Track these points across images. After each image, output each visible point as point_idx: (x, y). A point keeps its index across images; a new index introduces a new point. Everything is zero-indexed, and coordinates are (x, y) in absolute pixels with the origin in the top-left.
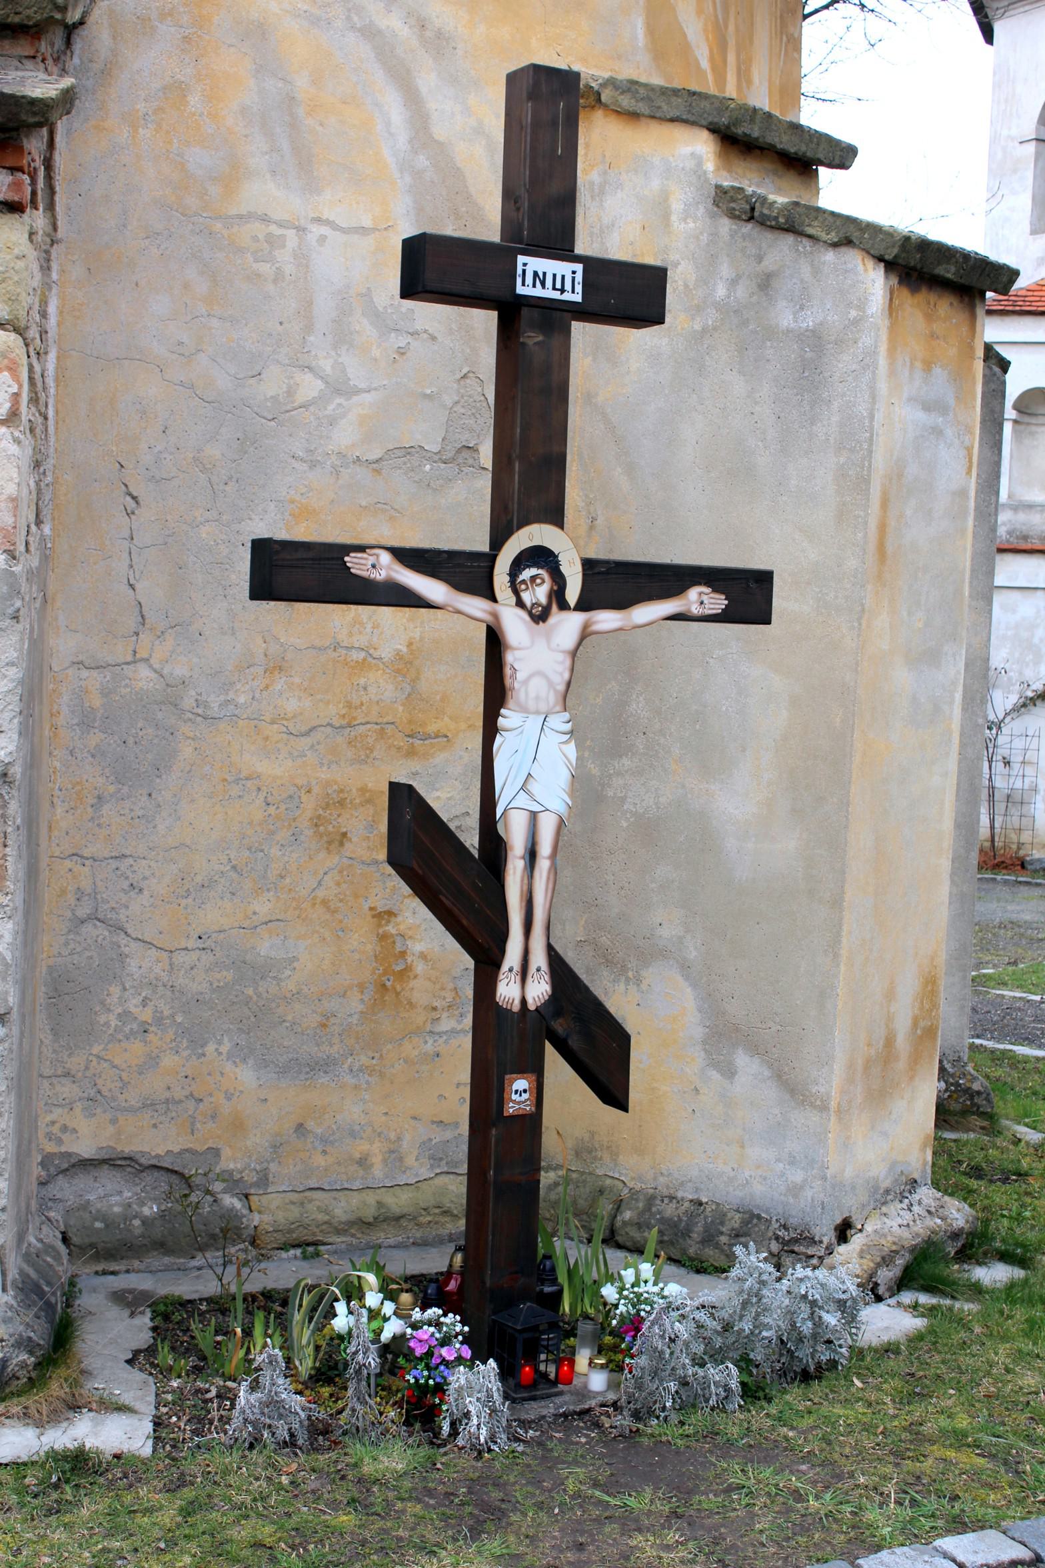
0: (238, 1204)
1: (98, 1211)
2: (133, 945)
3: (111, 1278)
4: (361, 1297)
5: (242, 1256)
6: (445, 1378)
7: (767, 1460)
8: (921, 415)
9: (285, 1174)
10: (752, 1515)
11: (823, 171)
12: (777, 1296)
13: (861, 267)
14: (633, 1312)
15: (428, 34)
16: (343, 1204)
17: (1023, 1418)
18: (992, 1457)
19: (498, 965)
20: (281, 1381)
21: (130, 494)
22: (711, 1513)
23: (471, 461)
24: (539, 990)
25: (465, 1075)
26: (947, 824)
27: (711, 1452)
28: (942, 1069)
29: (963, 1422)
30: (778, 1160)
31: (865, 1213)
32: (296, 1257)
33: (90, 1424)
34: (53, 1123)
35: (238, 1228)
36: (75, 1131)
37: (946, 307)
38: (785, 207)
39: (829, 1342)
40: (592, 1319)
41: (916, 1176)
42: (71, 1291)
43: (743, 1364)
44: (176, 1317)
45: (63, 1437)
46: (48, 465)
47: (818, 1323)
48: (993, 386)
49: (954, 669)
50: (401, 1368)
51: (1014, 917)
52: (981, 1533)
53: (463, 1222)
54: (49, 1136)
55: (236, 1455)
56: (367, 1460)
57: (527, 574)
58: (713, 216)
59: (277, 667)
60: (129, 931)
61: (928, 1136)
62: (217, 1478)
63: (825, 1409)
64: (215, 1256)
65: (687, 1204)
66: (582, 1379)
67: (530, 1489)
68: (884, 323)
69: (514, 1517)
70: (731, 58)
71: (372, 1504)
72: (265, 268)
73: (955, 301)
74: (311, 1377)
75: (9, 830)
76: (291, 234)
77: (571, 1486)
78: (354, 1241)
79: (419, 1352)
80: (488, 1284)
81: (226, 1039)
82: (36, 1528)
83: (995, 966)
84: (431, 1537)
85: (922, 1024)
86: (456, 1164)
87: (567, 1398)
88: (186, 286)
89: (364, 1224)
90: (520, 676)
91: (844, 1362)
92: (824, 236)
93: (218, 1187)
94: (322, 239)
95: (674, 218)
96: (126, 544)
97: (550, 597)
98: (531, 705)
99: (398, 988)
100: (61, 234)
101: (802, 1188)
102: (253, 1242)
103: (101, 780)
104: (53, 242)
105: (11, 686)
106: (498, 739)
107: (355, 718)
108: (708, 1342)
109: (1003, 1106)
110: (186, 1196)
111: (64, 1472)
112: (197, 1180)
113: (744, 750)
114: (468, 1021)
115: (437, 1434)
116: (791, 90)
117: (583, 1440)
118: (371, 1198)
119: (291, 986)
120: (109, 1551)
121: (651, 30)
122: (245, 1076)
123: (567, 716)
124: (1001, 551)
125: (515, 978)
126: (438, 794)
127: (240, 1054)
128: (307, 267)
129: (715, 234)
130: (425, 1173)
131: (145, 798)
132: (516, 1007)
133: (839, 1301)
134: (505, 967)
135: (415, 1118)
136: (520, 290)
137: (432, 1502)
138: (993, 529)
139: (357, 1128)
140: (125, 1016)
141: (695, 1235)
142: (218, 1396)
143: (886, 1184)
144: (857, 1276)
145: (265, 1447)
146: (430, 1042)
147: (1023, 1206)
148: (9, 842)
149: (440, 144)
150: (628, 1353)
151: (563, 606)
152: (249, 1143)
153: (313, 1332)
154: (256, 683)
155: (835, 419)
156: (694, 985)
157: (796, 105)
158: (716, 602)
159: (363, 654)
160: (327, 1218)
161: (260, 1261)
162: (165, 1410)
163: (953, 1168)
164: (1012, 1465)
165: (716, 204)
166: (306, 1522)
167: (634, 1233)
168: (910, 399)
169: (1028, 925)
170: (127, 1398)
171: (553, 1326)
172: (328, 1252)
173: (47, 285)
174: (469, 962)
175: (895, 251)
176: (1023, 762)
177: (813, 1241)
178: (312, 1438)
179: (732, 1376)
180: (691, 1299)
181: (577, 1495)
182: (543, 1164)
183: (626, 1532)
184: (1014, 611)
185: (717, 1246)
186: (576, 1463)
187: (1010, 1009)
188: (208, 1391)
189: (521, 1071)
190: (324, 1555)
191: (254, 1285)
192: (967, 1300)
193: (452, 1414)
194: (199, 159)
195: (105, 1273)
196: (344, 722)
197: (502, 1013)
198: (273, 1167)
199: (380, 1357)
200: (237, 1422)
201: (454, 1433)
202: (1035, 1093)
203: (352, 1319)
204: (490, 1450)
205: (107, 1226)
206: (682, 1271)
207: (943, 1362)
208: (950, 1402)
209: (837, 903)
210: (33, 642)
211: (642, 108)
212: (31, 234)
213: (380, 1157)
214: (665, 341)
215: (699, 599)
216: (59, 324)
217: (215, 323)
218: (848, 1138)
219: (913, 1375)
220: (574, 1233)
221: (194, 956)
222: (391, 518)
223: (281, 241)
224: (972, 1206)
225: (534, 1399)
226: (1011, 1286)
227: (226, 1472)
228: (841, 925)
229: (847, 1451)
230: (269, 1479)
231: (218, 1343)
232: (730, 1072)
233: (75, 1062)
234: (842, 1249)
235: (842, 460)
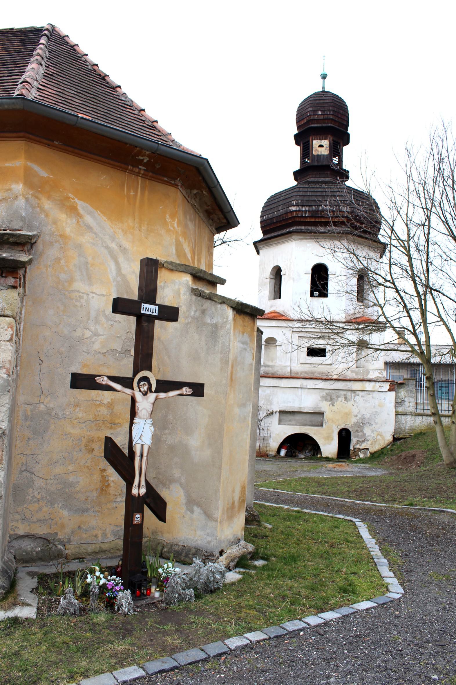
0: (62, 548)
1: (24, 550)
2: (36, 478)
3: (27, 568)
4: (95, 573)
5: (63, 562)
6: (116, 595)
7: (201, 615)
8: (241, 345)
9: (75, 539)
10: (197, 630)
11: (218, 285)
12: (204, 571)
13: (227, 309)
14: (166, 576)
15: (122, 248)
16: (90, 547)
17: (266, 601)
18: (259, 611)
19: (132, 484)
20: (72, 597)
21: (40, 360)
22: (186, 630)
23: (129, 354)
24: (143, 491)
25: (123, 513)
26: (248, 447)
27: (186, 613)
28: (247, 510)
29: (251, 603)
30: (205, 535)
31: (227, 548)
32: (77, 562)
33: (19, 609)
34: (13, 526)
35: (62, 554)
36: (18, 528)
37: (247, 319)
38: (209, 294)
39: (217, 582)
40: (156, 578)
41: (240, 538)
42: (16, 572)
43: (195, 589)
44: (44, 579)
45: (11, 614)
46: (20, 352)
47: (215, 577)
48: (259, 338)
49: (249, 408)
50: (105, 592)
51: (265, 469)
52: (256, 632)
53: (122, 552)
54: (12, 529)
55: (59, 617)
56: (95, 618)
57: (142, 383)
58: (191, 295)
59: (77, 405)
60: (35, 474)
61: (243, 528)
62: (54, 624)
63: (216, 600)
64: (55, 562)
65: (181, 547)
66: (153, 594)
67: (138, 625)
68: (232, 323)
69: (134, 633)
70: (196, 257)
71: (96, 630)
72: (78, 304)
73: (250, 318)
74: (80, 595)
75: (4, 447)
76: (85, 296)
77: (149, 624)
78: (93, 557)
79: (109, 588)
80: (128, 569)
81: (60, 503)
82: (3, 640)
83: (260, 482)
84: (112, 639)
85: (241, 499)
86: (121, 536)
87: (149, 599)
88: (58, 308)
89: (95, 553)
90: (139, 409)
91: (221, 588)
92: (218, 301)
93: (57, 543)
94: (93, 297)
95: (181, 295)
96: (39, 372)
97: (148, 389)
98: (142, 417)
99: (106, 490)
100: (26, 293)
101: (211, 542)
102: (66, 558)
103: (29, 434)
104: (24, 296)
105: (6, 409)
106: (134, 426)
107: (97, 419)
108: (186, 583)
109: (262, 519)
110: (48, 546)
111: (11, 624)
112: (51, 541)
113: (197, 428)
114: (124, 498)
115: (114, 610)
116: (210, 265)
117: (153, 611)
118: (98, 546)
119: (78, 489)
120: (23, 646)
121: (177, 250)
122: (65, 513)
123: (151, 420)
124: (261, 377)
125: (137, 488)
126: (118, 439)
127: (64, 507)
128: (89, 304)
129: (191, 300)
130: (112, 539)
131: (41, 438)
132: (137, 495)
133: (220, 572)
134: (134, 485)
135: (110, 524)
136: (142, 312)
137: (112, 629)
138: (259, 373)
139: (95, 527)
140: (33, 497)
141: (183, 555)
142: (55, 601)
143: (232, 540)
144: (225, 565)
145: (67, 615)
146: (114, 504)
147: (267, 545)
148: (4, 451)
149: (124, 275)
150: (165, 587)
151: (151, 392)
152: (65, 531)
153: (81, 583)
154: (71, 409)
155: (220, 346)
156: (184, 489)
157: (212, 268)
158: (190, 391)
159: (99, 402)
160: (86, 551)
161: (67, 563)
162: (40, 605)
163: (249, 535)
164: (263, 613)
165: (192, 292)
166: (78, 636)
167: (168, 555)
168: (238, 341)
169: (269, 471)
170: (30, 602)
171: (146, 580)
172: (86, 561)
173: (22, 306)
175: (235, 305)
176: (267, 430)
177: (213, 556)
178: (80, 612)
179: (192, 592)
180: (182, 572)
181: (151, 626)
182: (143, 536)
183: (164, 636)
184: (265, 392)
185: (189, 557)
186: (151, 617)
187: (264, 493)
188: (52, 599)
189: (138, 512)
190: (82, 645)
191: (66, 570)
192: (253, 570)
193: (118, 605)
194: (63, 276)
195: (25, 567)
196: (94, 420)
197: (133, 497)
199: (99, 589)
200: (60, 608)
201: (119, 610)
202: (270, 515)
203: (92, 579)
204: (128, 614)
205: (26, 554)
206: (180, 564)
207: (247, 587)
208: (248, 597)
209: (220, 468)
210: (13, 398)
211: (174, 268)
212: (19, 294)
213: (100, 535)
214: (178, 325)
215: (185, 390)
216: (25, 316)
217: (65, 317)
218: (223, 528)
219: (239, 590)
220: (151, 555)
221: (52, 481)
222: (108, 367)
224: (254, 545)
225: (140, 600)
226: (264, 566)
227: (56, 622)
228: (221, 474)
229: (222, 611)
230: (68, 624)
231: (56, 586)
232: (192, 512)
233: (20, 509)
234: (221, 558)
235: (222, 356)
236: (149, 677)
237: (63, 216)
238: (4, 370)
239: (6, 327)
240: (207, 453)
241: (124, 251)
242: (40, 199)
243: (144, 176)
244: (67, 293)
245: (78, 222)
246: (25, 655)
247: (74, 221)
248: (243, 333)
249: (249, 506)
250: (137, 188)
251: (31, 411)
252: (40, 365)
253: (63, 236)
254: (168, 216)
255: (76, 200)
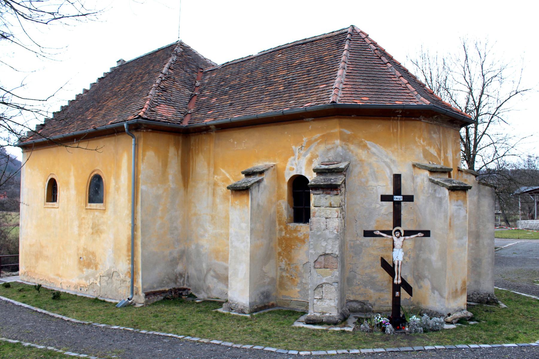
0: (371, 307)
8: (456, 207)
9: (377, 304)
24: (400, 282)
37: (460, 193)
42: (349, 316)
45: (343, 329)
54: (347, 297)
57: (396, 233)
72: (372, 192)
76: (375, 188)
85: (463, 288)
94: (379, 188)
95: (425, 182)
122: (372, 291)
127: (371, 288)
129: (429, 184)
132: (397, 283)
134: (395, 279)
140: (356, 283)
151: (401, 236)
158: (422, 235)
174: (392, 278)
194: (363, 180)
198: (376, 303)
209: (446, 271)
211: (420, 167)
223: (374, 188)
232: (434, 293)
233: (350, 288)
236: (386, 353)
237: (360, 151)
238: (336, 230)
239: (335, 212)
240: (440, 263)
241: (393, 162)
242: (348, 145)
243: (401, 120)
244: (366, 188)
245: (368, 152)
246: (345, 341)
247: (366, 152)
248: (457, 200)
249: (491, 294)
250: (398, 127)
251: (353, 244)
252: (356, 223)
253: (361, 161)
254: (417, 138)
255: (366, 142)
